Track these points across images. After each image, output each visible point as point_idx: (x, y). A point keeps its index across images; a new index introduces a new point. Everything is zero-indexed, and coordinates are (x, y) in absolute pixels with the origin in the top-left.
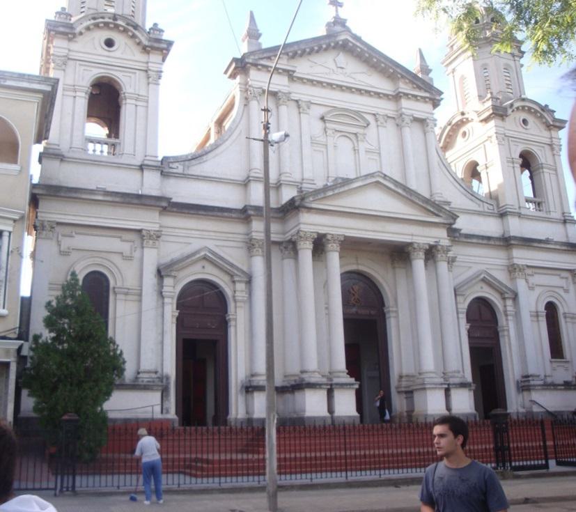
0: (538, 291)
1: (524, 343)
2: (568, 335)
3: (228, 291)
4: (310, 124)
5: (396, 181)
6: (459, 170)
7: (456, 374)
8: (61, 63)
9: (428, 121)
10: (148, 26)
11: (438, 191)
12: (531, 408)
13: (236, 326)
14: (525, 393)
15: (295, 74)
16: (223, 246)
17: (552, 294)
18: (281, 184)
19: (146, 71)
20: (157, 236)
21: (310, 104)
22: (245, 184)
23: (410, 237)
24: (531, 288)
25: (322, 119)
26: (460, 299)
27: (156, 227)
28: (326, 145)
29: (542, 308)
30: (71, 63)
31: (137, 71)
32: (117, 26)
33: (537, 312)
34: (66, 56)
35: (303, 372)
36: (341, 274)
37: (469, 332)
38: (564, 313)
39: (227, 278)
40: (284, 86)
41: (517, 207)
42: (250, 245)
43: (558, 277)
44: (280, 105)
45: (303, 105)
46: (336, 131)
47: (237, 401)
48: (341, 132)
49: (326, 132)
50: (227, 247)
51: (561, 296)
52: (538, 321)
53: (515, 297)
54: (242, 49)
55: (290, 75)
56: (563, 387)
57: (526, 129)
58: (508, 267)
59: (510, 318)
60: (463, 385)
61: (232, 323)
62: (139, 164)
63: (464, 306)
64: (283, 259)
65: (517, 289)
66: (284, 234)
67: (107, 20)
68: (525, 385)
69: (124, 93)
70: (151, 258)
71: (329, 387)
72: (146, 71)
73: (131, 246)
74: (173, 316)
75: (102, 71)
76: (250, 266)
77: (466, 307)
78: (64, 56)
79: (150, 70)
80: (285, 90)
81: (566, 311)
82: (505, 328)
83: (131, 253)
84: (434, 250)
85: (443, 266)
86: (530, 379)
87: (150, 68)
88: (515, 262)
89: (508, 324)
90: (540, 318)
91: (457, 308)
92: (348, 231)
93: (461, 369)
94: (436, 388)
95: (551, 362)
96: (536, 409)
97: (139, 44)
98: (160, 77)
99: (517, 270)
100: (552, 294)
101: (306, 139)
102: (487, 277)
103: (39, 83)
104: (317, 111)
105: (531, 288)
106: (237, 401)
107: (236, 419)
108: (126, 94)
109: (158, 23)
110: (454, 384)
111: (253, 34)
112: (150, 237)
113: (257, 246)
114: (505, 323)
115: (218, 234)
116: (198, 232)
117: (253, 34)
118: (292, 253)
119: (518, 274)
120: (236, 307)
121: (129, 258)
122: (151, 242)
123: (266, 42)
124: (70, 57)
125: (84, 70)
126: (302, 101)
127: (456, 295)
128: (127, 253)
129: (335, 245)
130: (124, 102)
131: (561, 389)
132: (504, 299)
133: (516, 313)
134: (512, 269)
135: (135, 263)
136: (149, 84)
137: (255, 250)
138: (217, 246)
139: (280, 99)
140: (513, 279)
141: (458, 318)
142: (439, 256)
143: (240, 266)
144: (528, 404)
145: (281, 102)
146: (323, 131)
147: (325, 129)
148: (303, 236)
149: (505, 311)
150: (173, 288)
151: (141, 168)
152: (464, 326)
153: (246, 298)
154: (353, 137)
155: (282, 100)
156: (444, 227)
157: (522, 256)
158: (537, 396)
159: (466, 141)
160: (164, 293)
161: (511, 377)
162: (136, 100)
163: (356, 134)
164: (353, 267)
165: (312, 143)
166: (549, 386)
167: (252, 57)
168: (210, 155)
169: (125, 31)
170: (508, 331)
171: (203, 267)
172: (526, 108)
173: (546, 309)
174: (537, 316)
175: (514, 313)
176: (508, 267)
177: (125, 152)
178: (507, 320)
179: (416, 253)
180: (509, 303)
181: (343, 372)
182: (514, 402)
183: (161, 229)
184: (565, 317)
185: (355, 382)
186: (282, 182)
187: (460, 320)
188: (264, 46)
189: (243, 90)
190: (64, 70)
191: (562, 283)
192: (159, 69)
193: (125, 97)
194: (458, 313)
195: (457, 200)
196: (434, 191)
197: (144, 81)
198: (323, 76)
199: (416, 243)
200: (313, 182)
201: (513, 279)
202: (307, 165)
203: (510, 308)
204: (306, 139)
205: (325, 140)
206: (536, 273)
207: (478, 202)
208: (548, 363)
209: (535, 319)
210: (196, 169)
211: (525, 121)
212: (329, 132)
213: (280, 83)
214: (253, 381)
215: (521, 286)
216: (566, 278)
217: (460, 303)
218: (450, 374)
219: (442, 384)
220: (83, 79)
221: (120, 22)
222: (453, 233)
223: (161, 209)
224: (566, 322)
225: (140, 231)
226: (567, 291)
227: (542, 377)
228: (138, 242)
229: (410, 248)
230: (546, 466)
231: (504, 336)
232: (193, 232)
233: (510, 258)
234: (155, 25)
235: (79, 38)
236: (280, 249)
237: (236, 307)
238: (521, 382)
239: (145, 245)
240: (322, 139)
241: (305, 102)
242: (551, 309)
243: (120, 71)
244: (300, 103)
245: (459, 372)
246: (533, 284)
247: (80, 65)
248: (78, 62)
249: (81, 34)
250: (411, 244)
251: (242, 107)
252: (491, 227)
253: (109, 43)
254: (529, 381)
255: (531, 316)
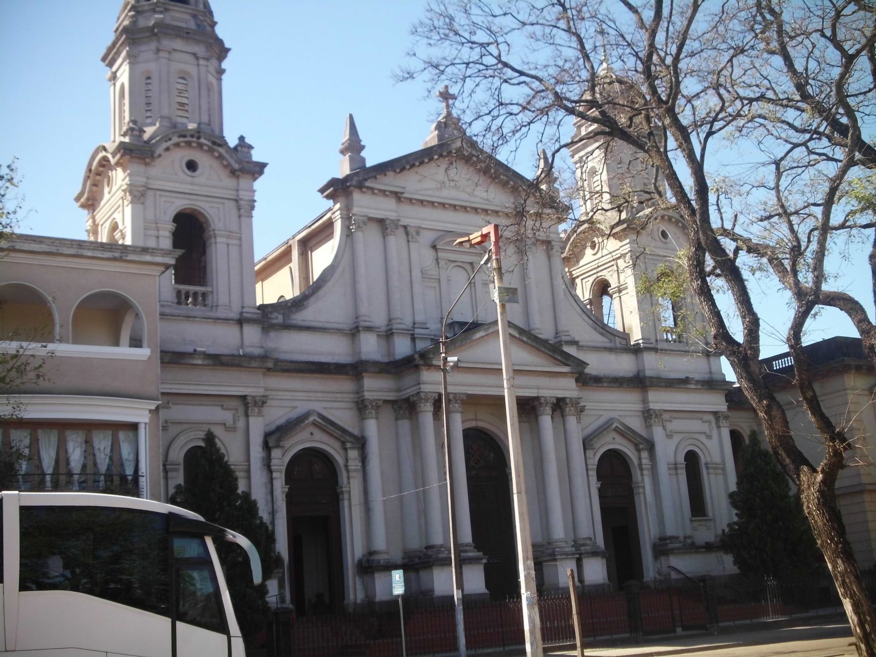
0: (677, 438)
1: (661, 502)
2: (710, 488)
3: (339, 458)
4: (422, 255)
5: (520, 328)
6: (584, 291)
7: (588, 542)
8: (138, 194)
9: (553, 243)
10: (232, 142)
11: (565, 329)
12: (670, 575)
13: (350, 499)
14: (663, 559)
15: (403, 195)
16: (331, 408)
17: (692, 441)
18: (393, 333)
19: (236, 200)
20: (261, 403)
21: (419, 230)
22: (354, 332)
23: (536, 391)
24: (669, 436)
25: (434, 247)
26: (590, 453)
27: (260, 392)
28: (439, 280)
29: (681, 459)
30: (151, 193)
31: (226, 201)
32: (200, 146)
33: (676, 464)
34: (145, 186)
35: (428, 547)
36: (464, 431)
37: (600, 490)
38: (706, 464)
39: (337, 445)
40: (392, 211)
41: (653, 340)
42: (361, 407)
43: (700, 421)
44: (387, 235)
45: (412, 231)
46: (450, 261)
47: (355, 584)
48: (455, 261)
49: (438, 263)
50: (338, 408)
51: (703, 444)
52: (677, 474)
53: (651, 446)
54: (342, 168)
55: (398, 196)
56: (704, 550)
57: (666, 243)
58: (643, 412)
59: (645, 472)
60: (594, 554)
61: (346, 496)
62: (237, 316)
63: (594, 461)
64: (397, 420)
65: (653, 438)
66: (398, 390)
67: (189, 139)
68: (662, 548)
69: (214, 230)
70: (258, 426)
71: (578, 556)
72: (236, 200)
73: (234, 415)
74: (283, 492)
75: (187, 202)
76: (362, 429)
77: (596, 463)
78: (142, 186)
79: (241, 199)
80: (392, 215)
81: (708, 460)
82: (640, 485)
83: (234, 423)
84: (561, 404)
85: (572, 421)
86: (668, 541)
87: (241, 197)
88: (651, 408)
89: (643, 480)
90: (679, 471)
91: (586, 465)
92: (471, 388)
93: (592, 537)
94: (567, 558)
95: (691, 521)
96: (674, 575)
97: (226, 167)
98: (252, 208)
99: (654, 416)
100: (692, 441)
101: (416, 273)
102: (619, 426)
103: (163, 256)
104: (427, 237)
105: (669, 436)
106: (355, 584)
107: (355, 603)
108: (216, 232)
109: (244, 136)
110: (586, 553)
111: (354, 146)
112: (256, 403)
113: (370, 407)
114: (640, 478)
115: (326, 395)
116: (303, 394)
117: (354, 146)
118: (407, 412)
119: (655, 421)
120: (349, 478)
121: (232, 429)
122: (256, 410)
123: (372, 157)
124: (151, 186)
125: (165, 201)
126: (411, 227)
127: (585, 449)
128: (230, 423)
129: (457, 405)
130: (213, 240)
131: (702, 552)
132: (639, 450)
133: (652, 466)
134: (648, 415)
135: (240, 435)
136: (240, 216)
137: (367, 412)
138: (325, 408)
139: (387, 228)
140: (648, 427)
141: (588, 476)
142: (567, 410)
143: (350, 430)
144: (665, 570)
145: (389, 231)
146: (435, 262)
147: (437, 260)
148: (423, 397)
149: (640, 465)
150: (281, 459)
151: (241, 322)
152: (595, 485)
153: (359, 467)
154: (468, 267)
155: (389, 229)
156: (572, 377)
157: (659, 400)
158: (676, 561)
159: (595, 255)
160: (272, 467)
161: (647, 540)
162: (228, 238)
163: (471, 264)
164: (472, 424)
165: (423, 277)
166: (692, 547)
167: (356, 178)
168: (312, 300)
169: (211, 151)
170: (644, 487)
171: (312, 434)
172: (666, 217)
173: (686, 459)
174: (676, 469)
175: (650, 466)
176: (643, 412)
177: (220, 303)
178: (642, 475)
179: (542, 409)
180: (645, 454)
181: (470, 546)
182: (651, 567)
183: (268, 393)
184: (707, 468)
185: (483, 557)
186: (394, 331)
187: (590, 478)
188: (369, 164)
189: (345, 217)
190: (143, 204)
191: (705, 427)
192: (251, 198)
193: (214, 234)
194: (587, 470)
195: (582, 331)
196: (560, 328)
197: (234, 212)
198: (430, 192)
199: (543, 397)
200: (425, 327)
201: (648, 427)
202: (418, 306)
203: (646, 461)
204: (416, 273)
205: (437, 273)
206: (675, 418)
207: (608, 335)
208: (688, 522)
209: (673, 472)
210: (299, 318)
211: (664, 234)
212: (442, 263)
213: (385, 208)
214: (373, 560)
215: (658, 434)
216: (710, 422)
217: (590, 458)
218: (581, 542)
219: (573, 554)
220: (165, 213)
221: (203, 141)
222: (585, 380)
223: (265, 370)
224: (708, 474)
225: (244, 398)
226: (709, 437)
227: (682, 539)
228: (241, 410)
229: (536, 403)
230: (675, 631)
231: (639, 493)
232: (299, 394)
233: (645, 401)
234: (242, 138)
235: (158, 161)
236: (393, 408)
237: (349, 478)
238: (659, 545)
239: (250, 414)
240: (434, 272)
241: (414, 227)
242: (692, 458)
243: (207, 202)
244: (409, 228)
245: (590, 539)
246: (671, 431)
247: (160, 195)
248: (158, 193)
249: (160, 156)
250: (537, 398)
251: (345, 238)
252: (623, 365)
253: (192, 166)
254: (666, 544)
255: (669, 469)
